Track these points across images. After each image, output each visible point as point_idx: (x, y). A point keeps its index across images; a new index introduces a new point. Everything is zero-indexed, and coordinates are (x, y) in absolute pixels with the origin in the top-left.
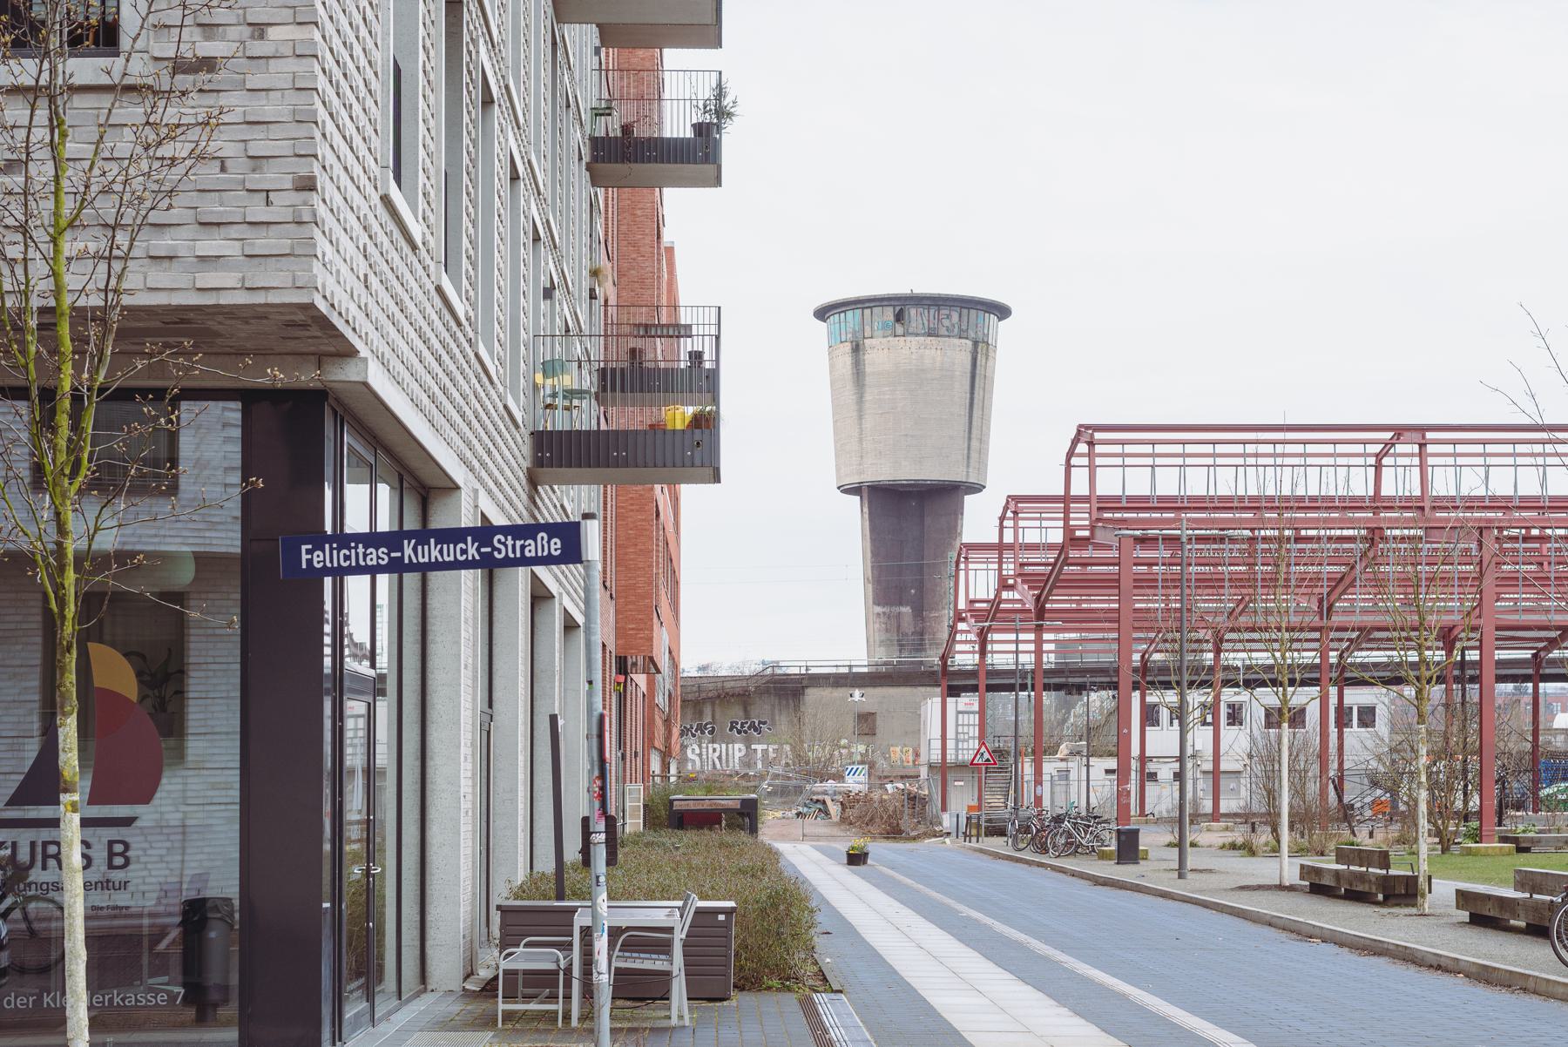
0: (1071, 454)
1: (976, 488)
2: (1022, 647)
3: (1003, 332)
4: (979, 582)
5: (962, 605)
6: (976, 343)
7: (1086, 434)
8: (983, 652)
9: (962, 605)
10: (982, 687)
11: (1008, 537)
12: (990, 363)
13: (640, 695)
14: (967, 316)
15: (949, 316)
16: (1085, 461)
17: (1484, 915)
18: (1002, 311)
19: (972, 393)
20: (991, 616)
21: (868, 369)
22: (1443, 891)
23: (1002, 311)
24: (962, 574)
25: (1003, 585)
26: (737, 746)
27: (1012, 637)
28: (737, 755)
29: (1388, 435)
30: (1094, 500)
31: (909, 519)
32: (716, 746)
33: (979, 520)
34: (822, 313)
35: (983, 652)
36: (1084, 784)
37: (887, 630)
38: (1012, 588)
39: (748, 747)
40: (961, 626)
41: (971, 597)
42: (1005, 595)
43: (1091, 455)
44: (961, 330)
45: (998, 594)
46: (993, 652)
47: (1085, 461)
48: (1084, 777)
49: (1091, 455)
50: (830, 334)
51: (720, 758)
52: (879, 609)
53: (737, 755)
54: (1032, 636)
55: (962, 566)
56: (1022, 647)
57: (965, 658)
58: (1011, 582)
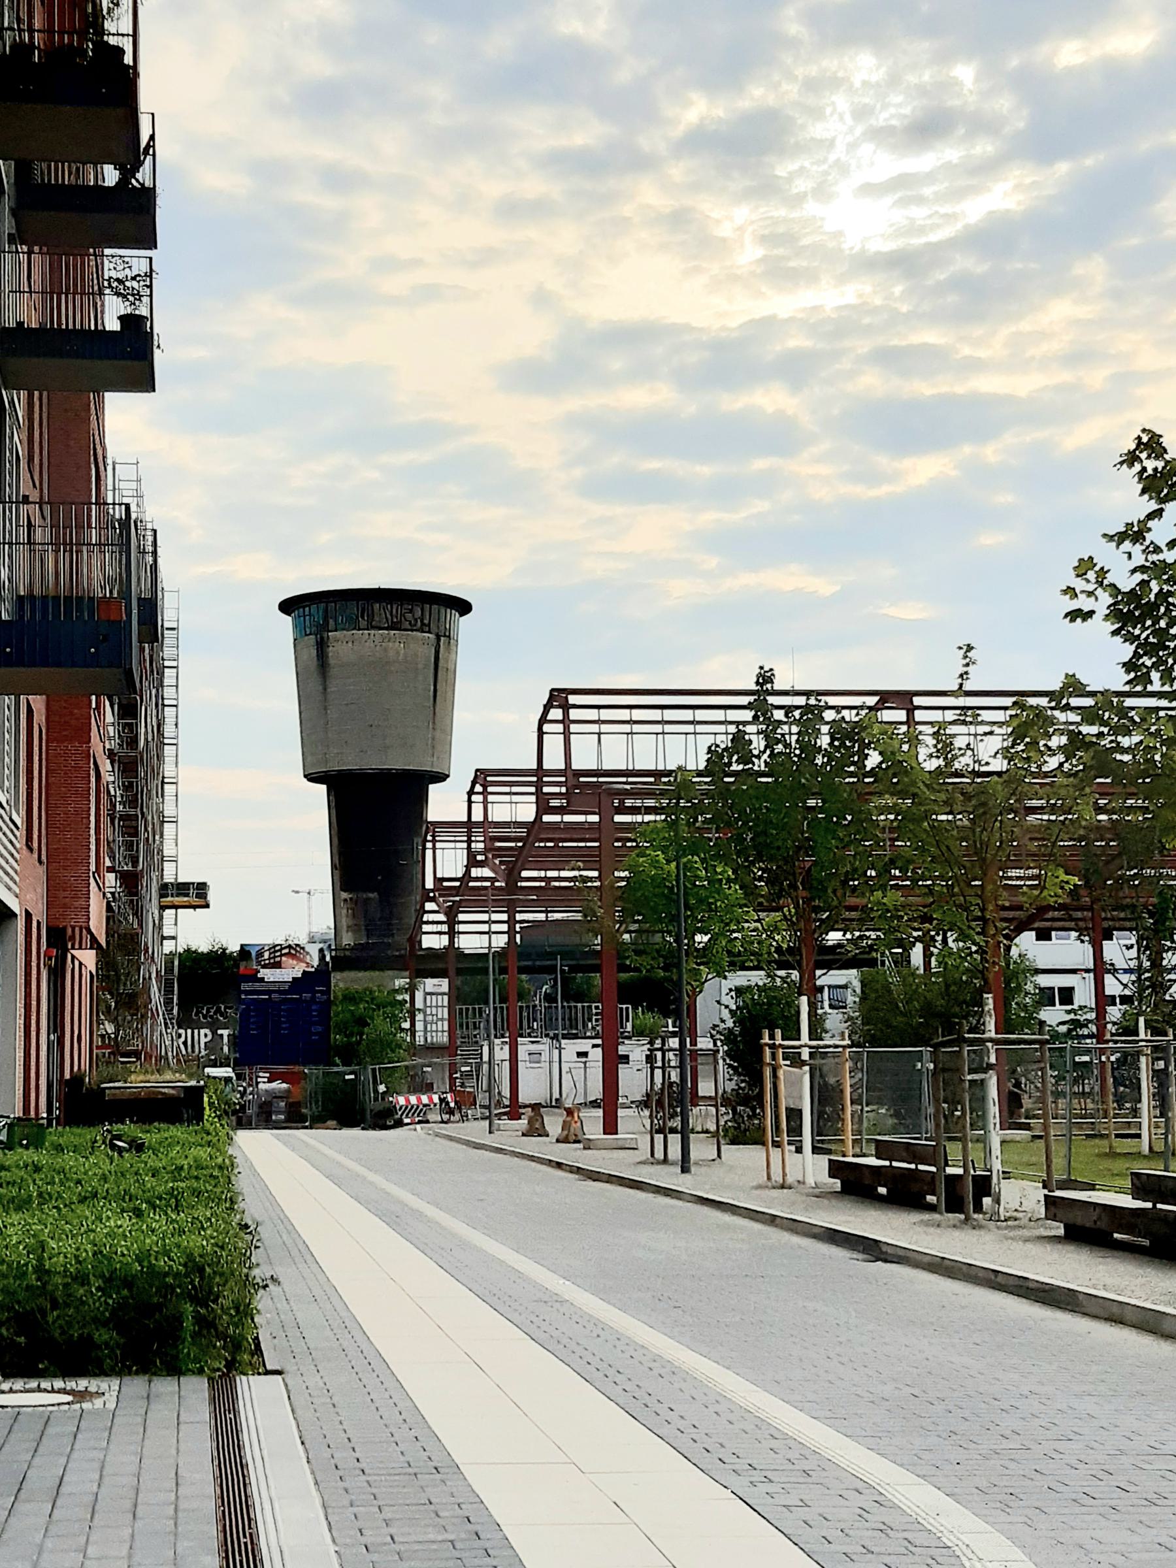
0: (543, 720)
1: (441, 777)
2: (434, 1004)
3: (464, 626)
4: (447, 861)
5: (429, 884)
6: (438, 637)
7: (558, 698)
8: (452, 934)
9: (429, 884)
10: (452, 972)
11: (478, 816)
12: (453, 656)
13: (86, 979)
14: (426, 613)
15: (411, 611)
16: (559, 728)
17: (1089, 1231)
18: (464, 607)
19: (435, 691)
20: (460, 896)
21: (332, 661)
22: (1021, 1195)
23: (464, 607)
24: (429, 853)
25: (472, 862)
26: (202, 1031)
27: (485, 917)
28: (203, 1040)
29: (872, 701)
30: (569, 773)
31: (374, 819)
32: (182, 1031)
33: (444, 803)
34: (286, 606)
35: (452, 934)
36: (556, 1066)
37: (354, 916)
38: (481, 864)
39: (214, 1033)
40: (429, 906)
41: (439, 875)
42: (475, 872)
43: (566, 721)
44: (423, 624)
45: (468, 869)
46: (459, 933)
47: (559, 728)
48: (556, 1058)
49: (566, 721)
50: (295, 626)
51: (185, 1043)
52: (344, 895)
53: (203, 1040)
54: (504, 917)
55: (429, 845)
56: (434, 1004)
57: (432, 941)
58: (479, 858)
